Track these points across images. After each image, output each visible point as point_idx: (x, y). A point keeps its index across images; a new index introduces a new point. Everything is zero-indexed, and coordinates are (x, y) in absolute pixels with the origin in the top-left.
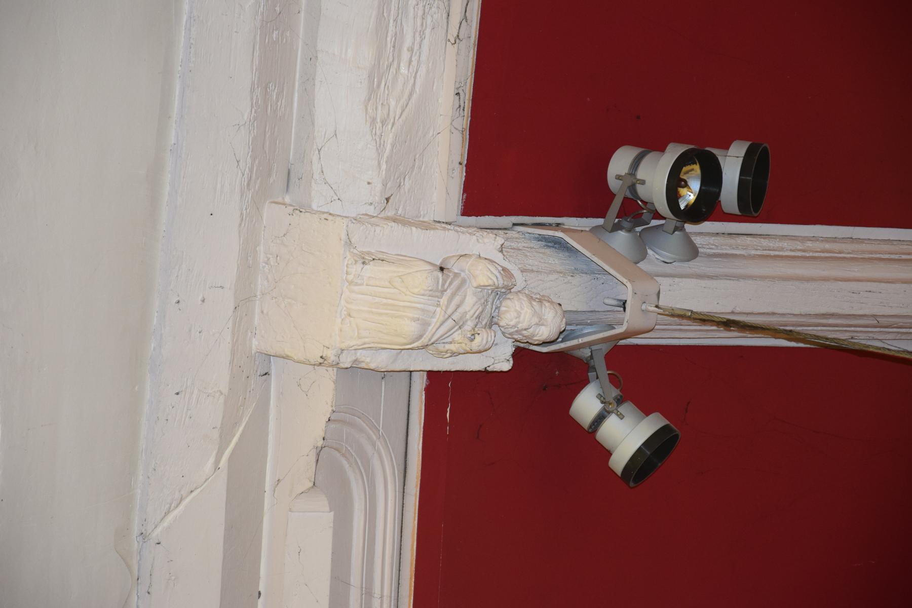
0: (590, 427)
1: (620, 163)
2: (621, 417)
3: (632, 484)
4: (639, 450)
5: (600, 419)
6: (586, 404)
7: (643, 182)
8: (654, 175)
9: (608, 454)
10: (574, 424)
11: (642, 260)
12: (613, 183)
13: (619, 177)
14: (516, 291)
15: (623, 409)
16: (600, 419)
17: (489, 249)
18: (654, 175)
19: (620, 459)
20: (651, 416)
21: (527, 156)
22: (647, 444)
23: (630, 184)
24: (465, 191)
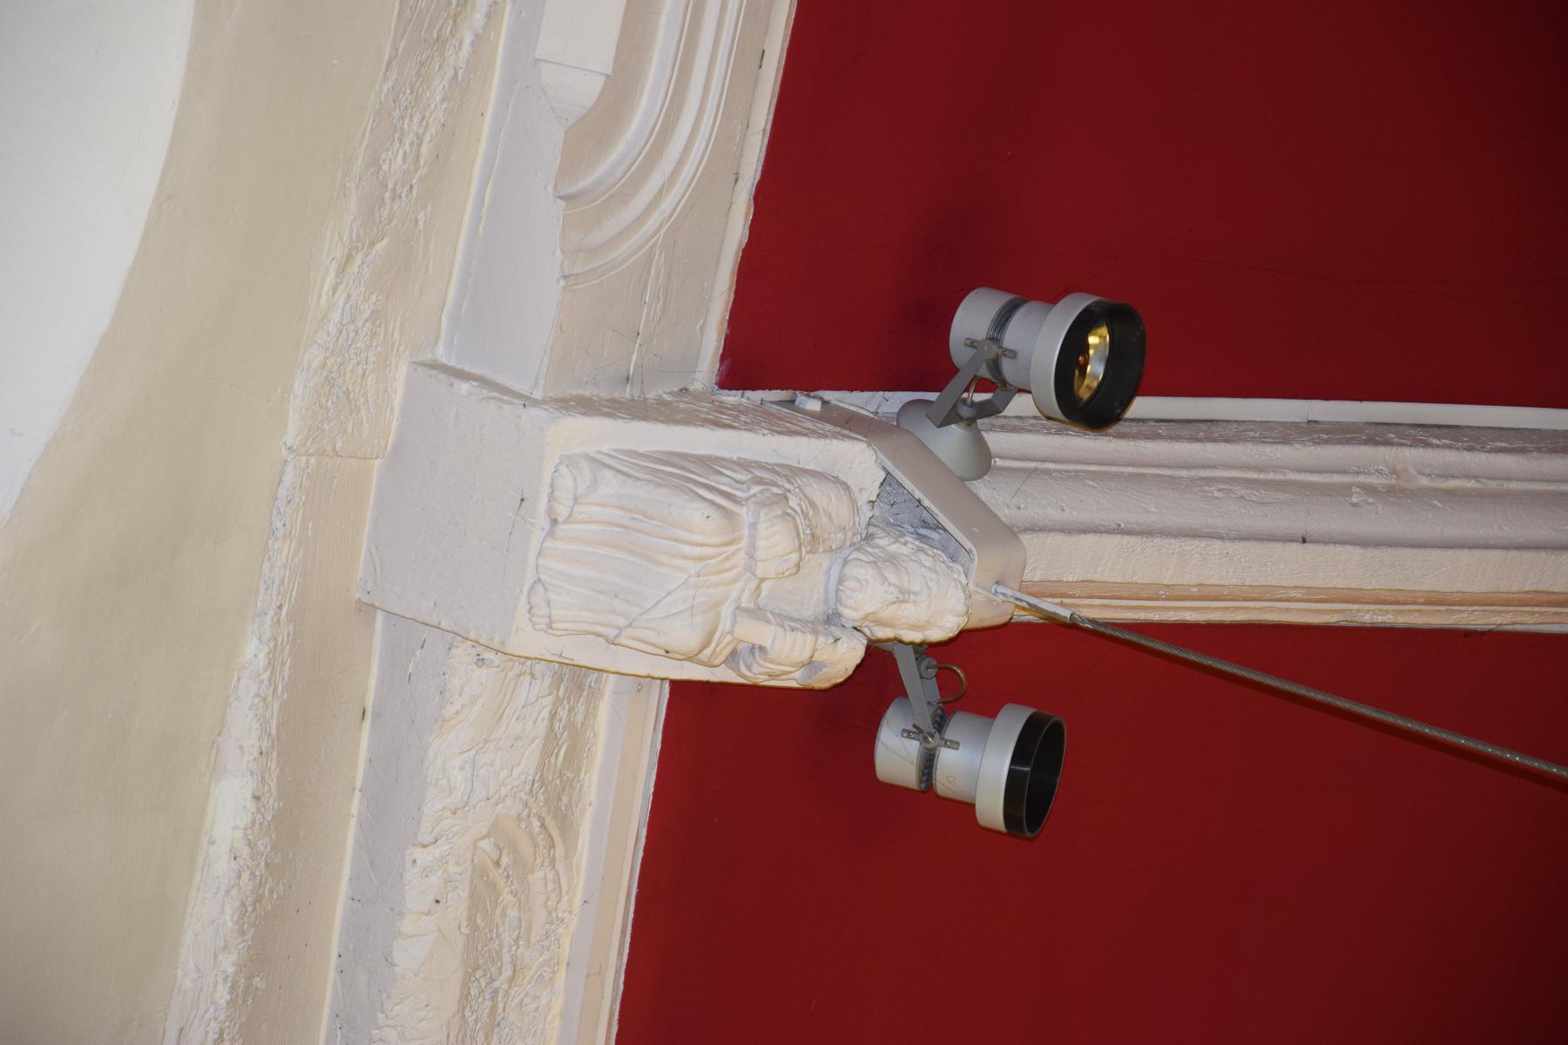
0: (921, 781)
1: (972, 319)
2: (954, 745)
3: (1028, 834)
4: (1011, 773)
5: (928, 764)
6: (895, 752)
7: (1013, 354)
8: (1038, 337)
9: (968, 807)
10: (896, 791)
11: (979, 477)
12: (958, 350)
13: (972, 344)
14: (820, 552)
15: (950, 733)
16: (928, 764)
17: (835, 456)
18: (1038, 337)
19: (991, 808)
20: (1000, 715)
21: (835, 300)
22: (1017, 758)
23: (992, 355)
24: (723, 358)
